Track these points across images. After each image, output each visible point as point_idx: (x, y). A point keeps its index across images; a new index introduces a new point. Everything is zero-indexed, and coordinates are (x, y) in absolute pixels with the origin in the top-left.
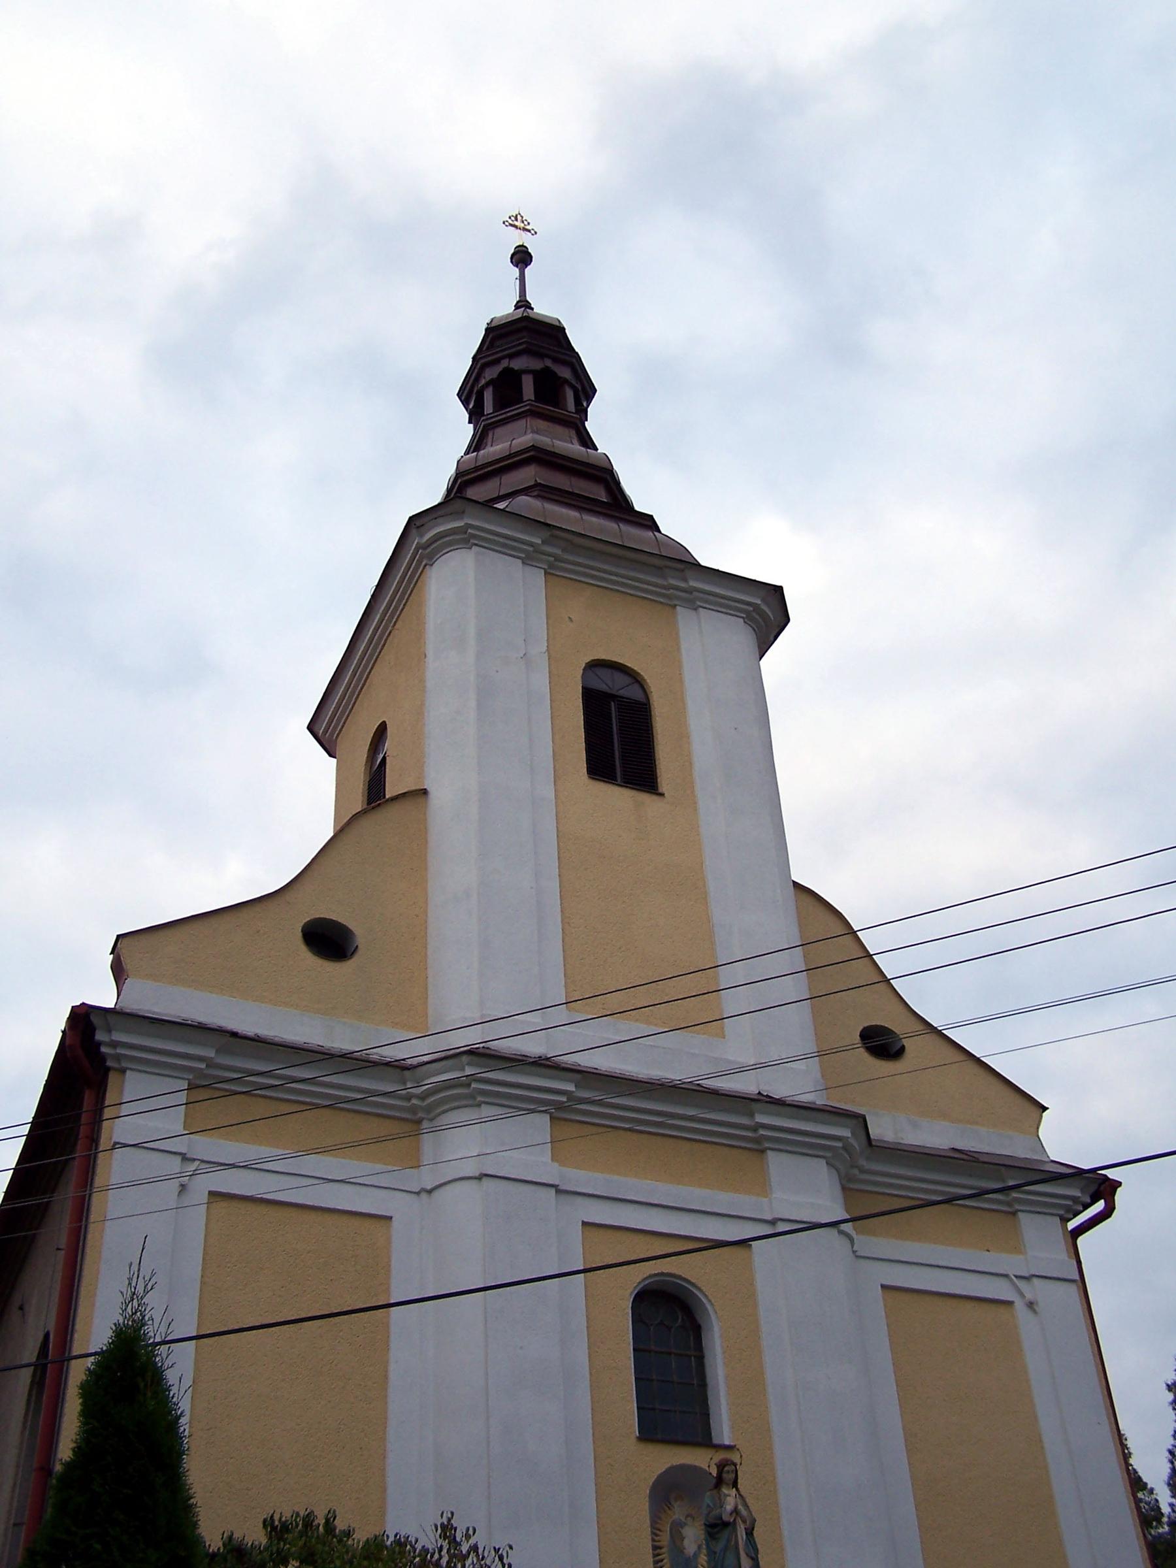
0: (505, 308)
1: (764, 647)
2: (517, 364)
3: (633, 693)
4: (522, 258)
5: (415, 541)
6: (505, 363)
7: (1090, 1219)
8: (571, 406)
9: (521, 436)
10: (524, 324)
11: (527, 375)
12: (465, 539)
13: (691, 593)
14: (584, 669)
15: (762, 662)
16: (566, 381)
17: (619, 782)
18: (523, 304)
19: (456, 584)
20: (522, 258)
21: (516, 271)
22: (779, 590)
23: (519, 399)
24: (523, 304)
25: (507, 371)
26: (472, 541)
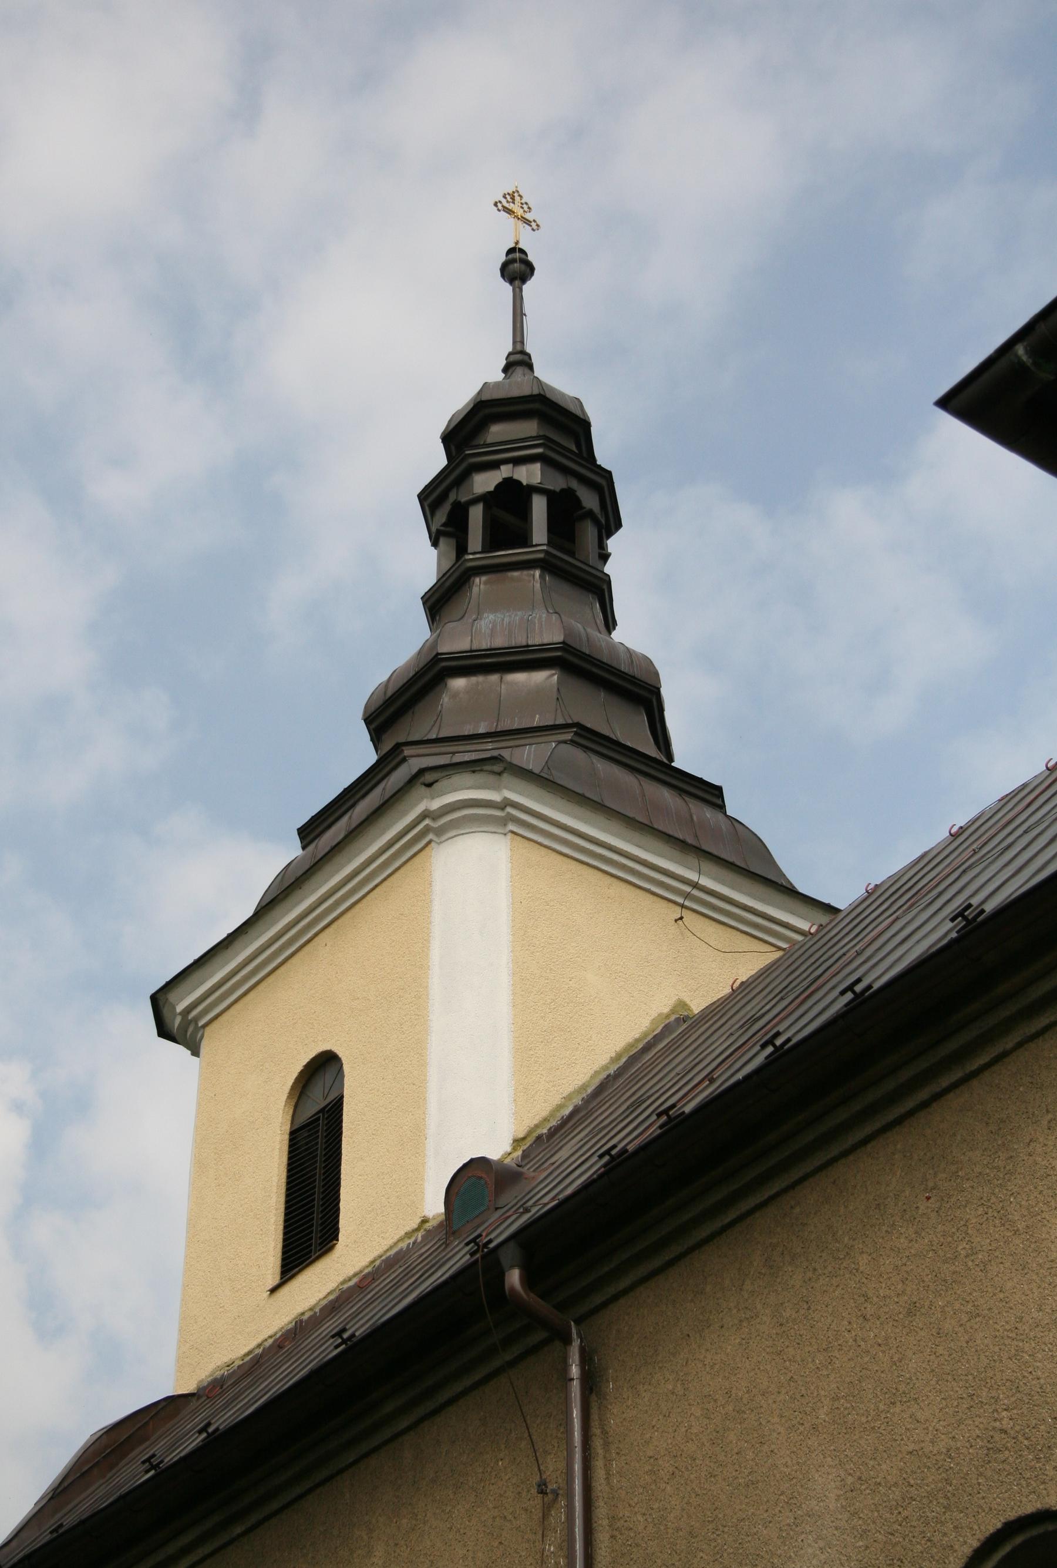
2: (530, 474)
4: (517, 269)
6: (505, 471)
9: (515, 612)
10: (537, 406)
13: (503, 809)
15: (730, 812)
18: (519, 361)
20: (517, 269)
21: (507, 289)
23: (523, 539)
24: (519, 361)
25: (509, 485)
26: (511, 827)
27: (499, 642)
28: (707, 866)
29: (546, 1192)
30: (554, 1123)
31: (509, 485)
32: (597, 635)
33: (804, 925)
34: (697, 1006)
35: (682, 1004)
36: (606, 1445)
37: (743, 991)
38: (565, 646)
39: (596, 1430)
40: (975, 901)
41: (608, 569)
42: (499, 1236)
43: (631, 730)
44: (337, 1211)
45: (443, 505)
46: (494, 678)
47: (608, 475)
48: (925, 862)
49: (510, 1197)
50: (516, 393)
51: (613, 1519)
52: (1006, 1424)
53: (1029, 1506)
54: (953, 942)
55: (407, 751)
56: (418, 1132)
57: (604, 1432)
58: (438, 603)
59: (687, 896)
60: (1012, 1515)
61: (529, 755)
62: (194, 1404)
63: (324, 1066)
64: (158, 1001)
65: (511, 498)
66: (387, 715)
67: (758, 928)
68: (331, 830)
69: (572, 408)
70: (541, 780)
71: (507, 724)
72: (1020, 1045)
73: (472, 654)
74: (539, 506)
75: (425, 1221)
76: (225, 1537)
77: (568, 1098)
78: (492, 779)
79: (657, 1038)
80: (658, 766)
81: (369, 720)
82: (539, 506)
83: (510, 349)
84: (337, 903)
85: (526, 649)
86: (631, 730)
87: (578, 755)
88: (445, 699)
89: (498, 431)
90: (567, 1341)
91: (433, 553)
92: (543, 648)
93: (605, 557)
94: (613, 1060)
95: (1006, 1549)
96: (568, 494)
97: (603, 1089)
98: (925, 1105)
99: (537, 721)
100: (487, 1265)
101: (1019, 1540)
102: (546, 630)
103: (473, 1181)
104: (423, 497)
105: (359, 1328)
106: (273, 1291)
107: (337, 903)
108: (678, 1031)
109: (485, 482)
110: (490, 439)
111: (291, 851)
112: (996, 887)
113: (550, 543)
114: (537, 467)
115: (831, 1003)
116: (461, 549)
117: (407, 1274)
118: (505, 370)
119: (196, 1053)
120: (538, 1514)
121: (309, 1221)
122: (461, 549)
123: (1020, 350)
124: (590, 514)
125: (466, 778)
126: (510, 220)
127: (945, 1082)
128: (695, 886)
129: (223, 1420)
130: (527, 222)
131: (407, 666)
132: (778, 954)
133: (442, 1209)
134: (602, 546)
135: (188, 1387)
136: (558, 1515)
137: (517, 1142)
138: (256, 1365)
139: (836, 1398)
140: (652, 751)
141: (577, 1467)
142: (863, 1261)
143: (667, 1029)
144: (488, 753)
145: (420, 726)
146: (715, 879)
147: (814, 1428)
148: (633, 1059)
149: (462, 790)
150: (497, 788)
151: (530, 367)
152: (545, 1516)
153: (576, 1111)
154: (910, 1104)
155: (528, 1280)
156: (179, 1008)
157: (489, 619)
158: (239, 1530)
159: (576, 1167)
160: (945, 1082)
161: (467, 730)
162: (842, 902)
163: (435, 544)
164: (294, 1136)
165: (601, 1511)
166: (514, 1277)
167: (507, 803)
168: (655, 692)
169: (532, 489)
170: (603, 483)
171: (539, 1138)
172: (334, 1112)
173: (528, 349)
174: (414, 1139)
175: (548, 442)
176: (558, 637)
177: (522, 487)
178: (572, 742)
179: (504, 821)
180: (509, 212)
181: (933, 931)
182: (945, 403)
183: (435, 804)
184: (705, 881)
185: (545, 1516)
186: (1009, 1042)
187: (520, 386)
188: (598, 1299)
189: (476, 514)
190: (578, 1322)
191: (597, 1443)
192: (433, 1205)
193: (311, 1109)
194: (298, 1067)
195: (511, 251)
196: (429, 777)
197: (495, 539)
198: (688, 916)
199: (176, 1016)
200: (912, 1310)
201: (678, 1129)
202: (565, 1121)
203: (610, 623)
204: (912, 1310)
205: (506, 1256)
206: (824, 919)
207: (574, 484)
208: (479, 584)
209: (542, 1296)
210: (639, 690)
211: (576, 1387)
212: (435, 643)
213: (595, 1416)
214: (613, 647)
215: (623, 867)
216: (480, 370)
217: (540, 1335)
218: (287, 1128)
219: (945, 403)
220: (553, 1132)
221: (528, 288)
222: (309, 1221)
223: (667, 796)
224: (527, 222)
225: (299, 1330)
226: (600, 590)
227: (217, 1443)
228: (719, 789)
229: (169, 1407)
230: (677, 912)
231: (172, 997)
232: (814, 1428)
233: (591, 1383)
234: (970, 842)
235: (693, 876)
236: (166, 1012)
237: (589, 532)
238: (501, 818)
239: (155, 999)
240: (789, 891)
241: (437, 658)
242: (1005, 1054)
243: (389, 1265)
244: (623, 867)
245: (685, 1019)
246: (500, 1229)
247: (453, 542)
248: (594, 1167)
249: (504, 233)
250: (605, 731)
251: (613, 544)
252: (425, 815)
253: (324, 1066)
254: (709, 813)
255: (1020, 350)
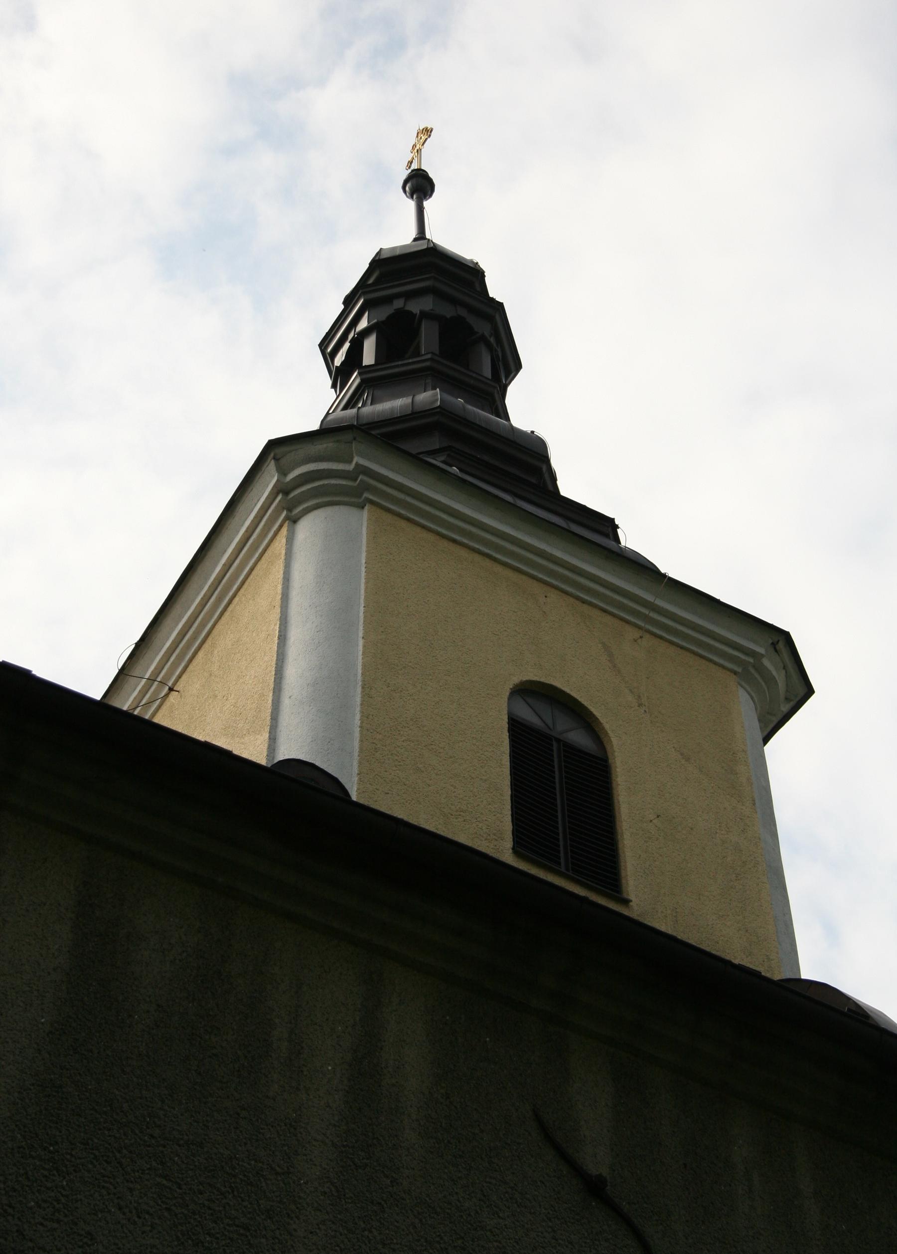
0: (399, 235)
1: (766, 740)
2: (415, 307)
3: (579, 738)
4: (420, 185)
5: (270, 479)
6: (398, 304)
7: (529, 544)
8: (487, 372)
11: (427, 329)
12: (352, 492)
14: (509, 699)
16: (483, 339)
17: (563, 869)
19: (311, 554)
22: (810, 691)
25: (401, 316)
26: (366, 495)
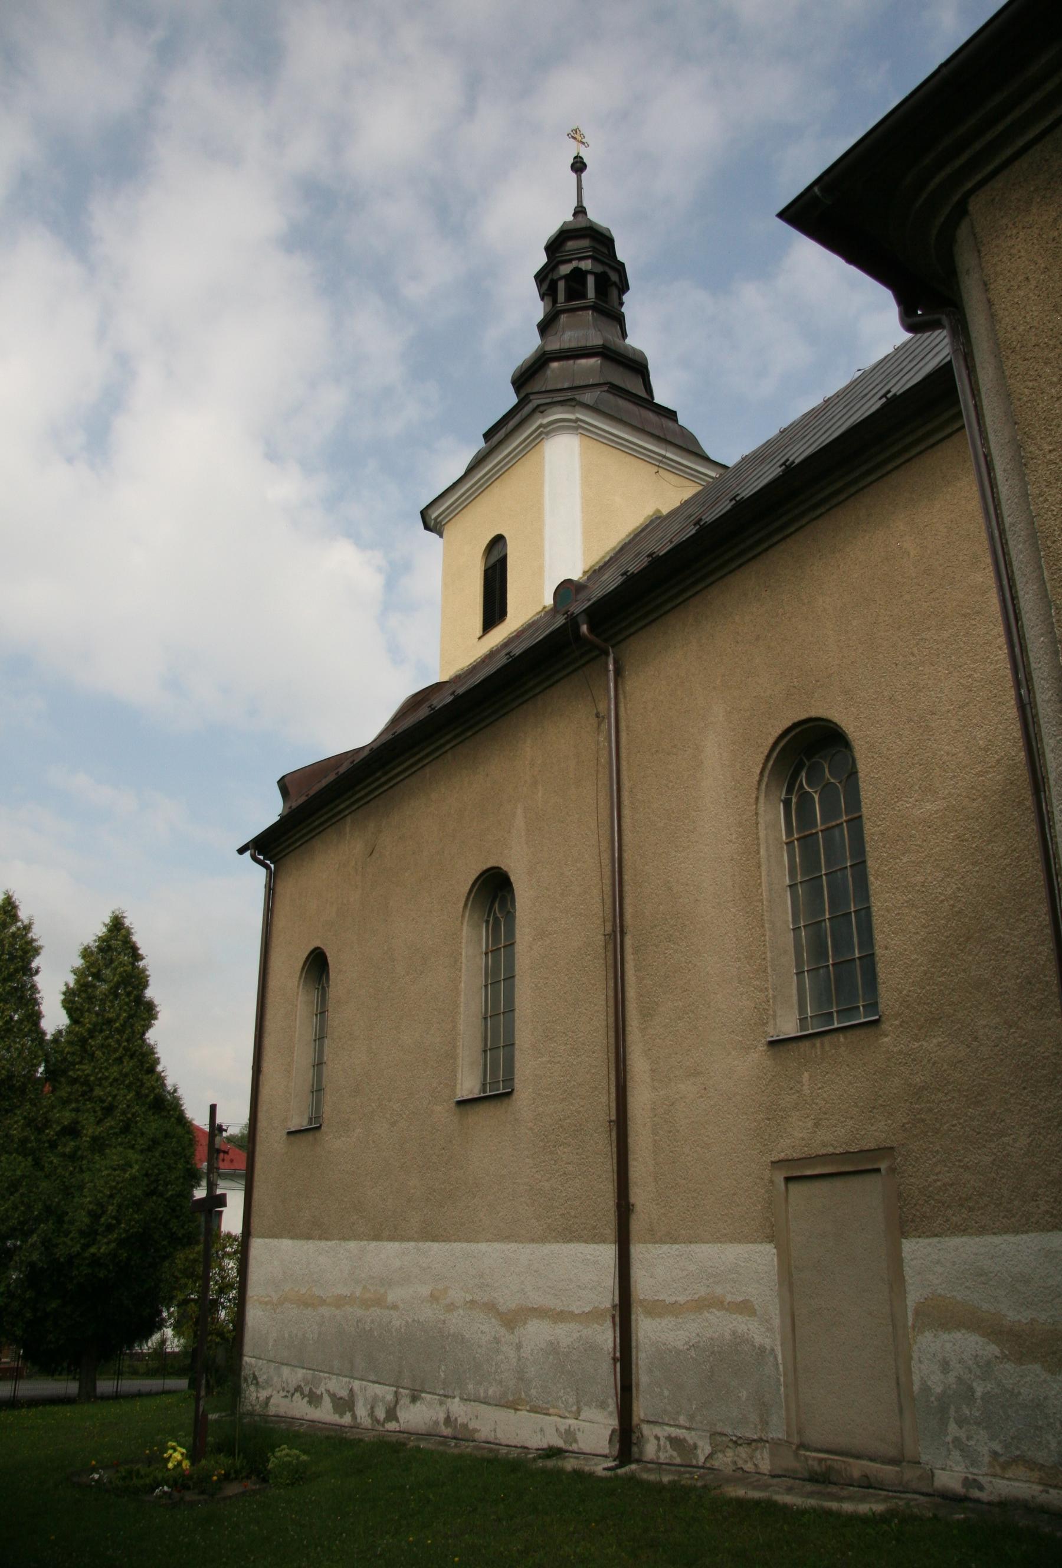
2: (586, 265)
4: (579, 166)
6: (575, 264)
9: (581, 330)
15: (680, 423)
18: (580, 211)
21: (574, 176)
23: (583, 296)
24: (580, 211)
26: (580, 431)
27: (573, 345)
28: (670, 448)
29: (597, 592)
30: (601, 564)
31: (576, 270)
32: (618, 341)
33: (713, 474)
34: (665, 511)
35: (658, 511)
36: (625, 697)
37: (686, 504)
38: (604, 346)
39: (621, 692)
40: (791, 459)
41: (623, 310)
42: (577, 611)
43: (634, 386)
44: (506, 604)
45: (545, 279)
46: (571, 362)
47: (622, 265)
48: (769, 444)
49: (583, 595)
50: (579, 226)
51: (628, 727)
52: (796, 684)
53: (804, 716)
54: (781, 476)
55: (532, 397)
56: (541, 569)
57: (624, 692)
58: (545, 327)
59: (661, 462)
60: (796, 720)
61: (588, 397)
62: (448, 685)
63: (498, 541)
64: (424, 514)
65: (578, 275)
66: (523, 380)
67: (693, 475)
68: (498, 435)
69: (605, 232)
70: (594, 409)
71: (577, 383)
72: (808, 523)
73: (561, 351)
74: (591, 280)
75: (545, 607)
76: (463, 737)
77: (608, 553)
78: (570, 408)
79: (647, 526)
80: (647, 401)
81: (514, 383)
82: (591, 280)
83: (576, 205)
84: (502, 468)
85: (585, 348)
86: (634, 386)
87: (611, 398)
88: (549, 372)
89: (571, 245)
90: (607, 654)
91: (541, 304)
92: (593, 347)
93: (622, 304)
94: (627, 536)
95: (793, 733)
96: (604, 274)
97: (623, 549)
98: (767, 550)
99: (591, 382)
100: (573, 622)
101: (798, 730)
102: (595, 339)
103: (566, 590)
104: (536, 277)
105: (517, 652)
106: (480, 638)
107: (502, 468)
108: (656, 522)
109: (565, 269)
110: (567, 249)
111: (481, 444)
112: (799, 453)
113: (596, 297)
114: (589, 262)
115: (725, 506)
116: (555, 301)
117: (537, 630)
118: (574, 215)
119: (441, 536)
120: (595, 725)
121: (494, 609)
122: (555, 301)
123: (816, 189)
124: (615, 283)
125: (560, 408)
126: (576, 143)
127: (775, 540)
128: (664, 457)
129: (461, 691)
130: (583, 143)
131: (530, 357)
132: (701, 488)
133: (552, 602)
134: (620, 299)
135: (445, 678)
136: (604, 726)
137: (585, 573)
138: (473, 669)
139: (724, 676)
140: (644, 395)
141: (612, 707)
142: (737, 618)
143: (652, 522)
144: (569, 397)
145: (538, 385)
146: (674, 454)
147: (714, 688)
148: (636, 535)
149: (557, 414)
150: (573, 413)
151: (585, 213)
152: (599, 727)
153: (611, 558)
154: (760, 549)
155: (591, 629)
156: (433, 516)
157: (568, 335)
158: (469, 734)
159: (611, 581)
160: (775, 540)
161: (559, 387)
162: (730, 463)
163: (542, 299)
164: (486, 572)
165: (623, 725)
166: (584, 628)
167: (578, 420)
168: (646, 367)
169: (587, 272)
170: (620, 268)
171: (595, 571)
172: (503, 562)
173: (585, 205)
174: (539, 572)
175: (594, 249)
176: (600, 342)
177: (583, 272)
178: (607, 391)
179: (577, 428)
180: (574, 138)
181: (772, 472)
182: (781, 215)
183: (545, 421)
184: (669, 455)
185: (599, 727)
186: (803, 522)
187: (581, 223)
188: (620, 637)
189: (561, 285)
190: (613, 647)
191: (621, 696)
192: (549, 601)
193: (493, 559)
194: (489, 539)
195: (576, 158)
196: (542, 409)
197: (570, 297)
198: (661, 471)
199: (432, 520)
200: (758, 638)
201: (657, 563)
202: (606, 564)
203: (624, 335)
204: (758, 638)
205: (581, 619)
206: (722, 471)
207: (607, 270)
208: (563, 318)
209: (597, 636)
210: (638, 366)
211: (611, 674)
212: (541, 348)
213: (620, 686)
214: (627, 347)
215: (632, 449)
216: (562, 215)
217: (596, 653)
218: (483, 568)
219: (781, 215)
220: (601, 568)
221: (583, 175)
222: (494, 609)
223: (651, 416)
224: (583, 143)
225: (491, 655)
226: (619, 320)
227: (458, 699)
228: (675, 412)
229: (438, 687)
230: (656, 469)
231: (430, 512)
232: (714, 688)
233: (618, 672)
234: (788, 435)
235: (663, 452)
236: (427, 519)
237: (615, 292)
238: (575, 427)
239: (422, 512)
240: (706, 459)
241: (544, 353)
242: (801, 527)
243: (531, 627)
244: (632, 449)
245: (659, 517)
246: (578, 607)
247: (551, 298)
248: (620, 580)
249: (571, 150)
250: (622, 385)
251: (626, 298)
252: (541, 426)
253: (498, 541)
254: (670, 424)
255: (816, 189)
